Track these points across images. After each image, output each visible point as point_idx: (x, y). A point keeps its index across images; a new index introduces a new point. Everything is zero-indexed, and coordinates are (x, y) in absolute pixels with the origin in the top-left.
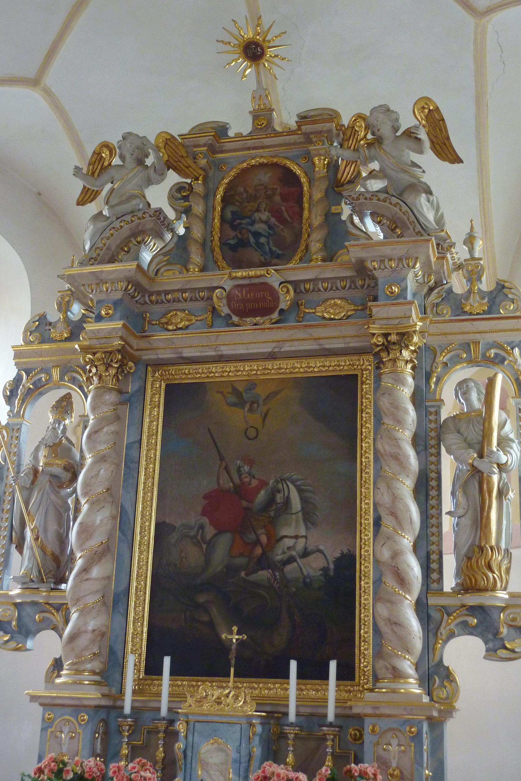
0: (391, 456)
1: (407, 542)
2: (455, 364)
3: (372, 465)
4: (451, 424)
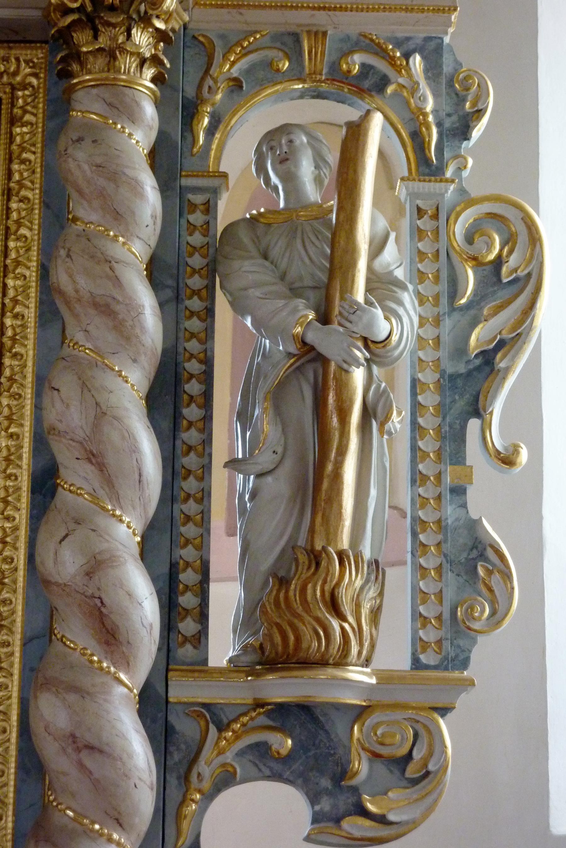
0: (96, 305)
1: (125, 531)
2: (262, 84)
3: (31, 336)
4: (245, 236)
